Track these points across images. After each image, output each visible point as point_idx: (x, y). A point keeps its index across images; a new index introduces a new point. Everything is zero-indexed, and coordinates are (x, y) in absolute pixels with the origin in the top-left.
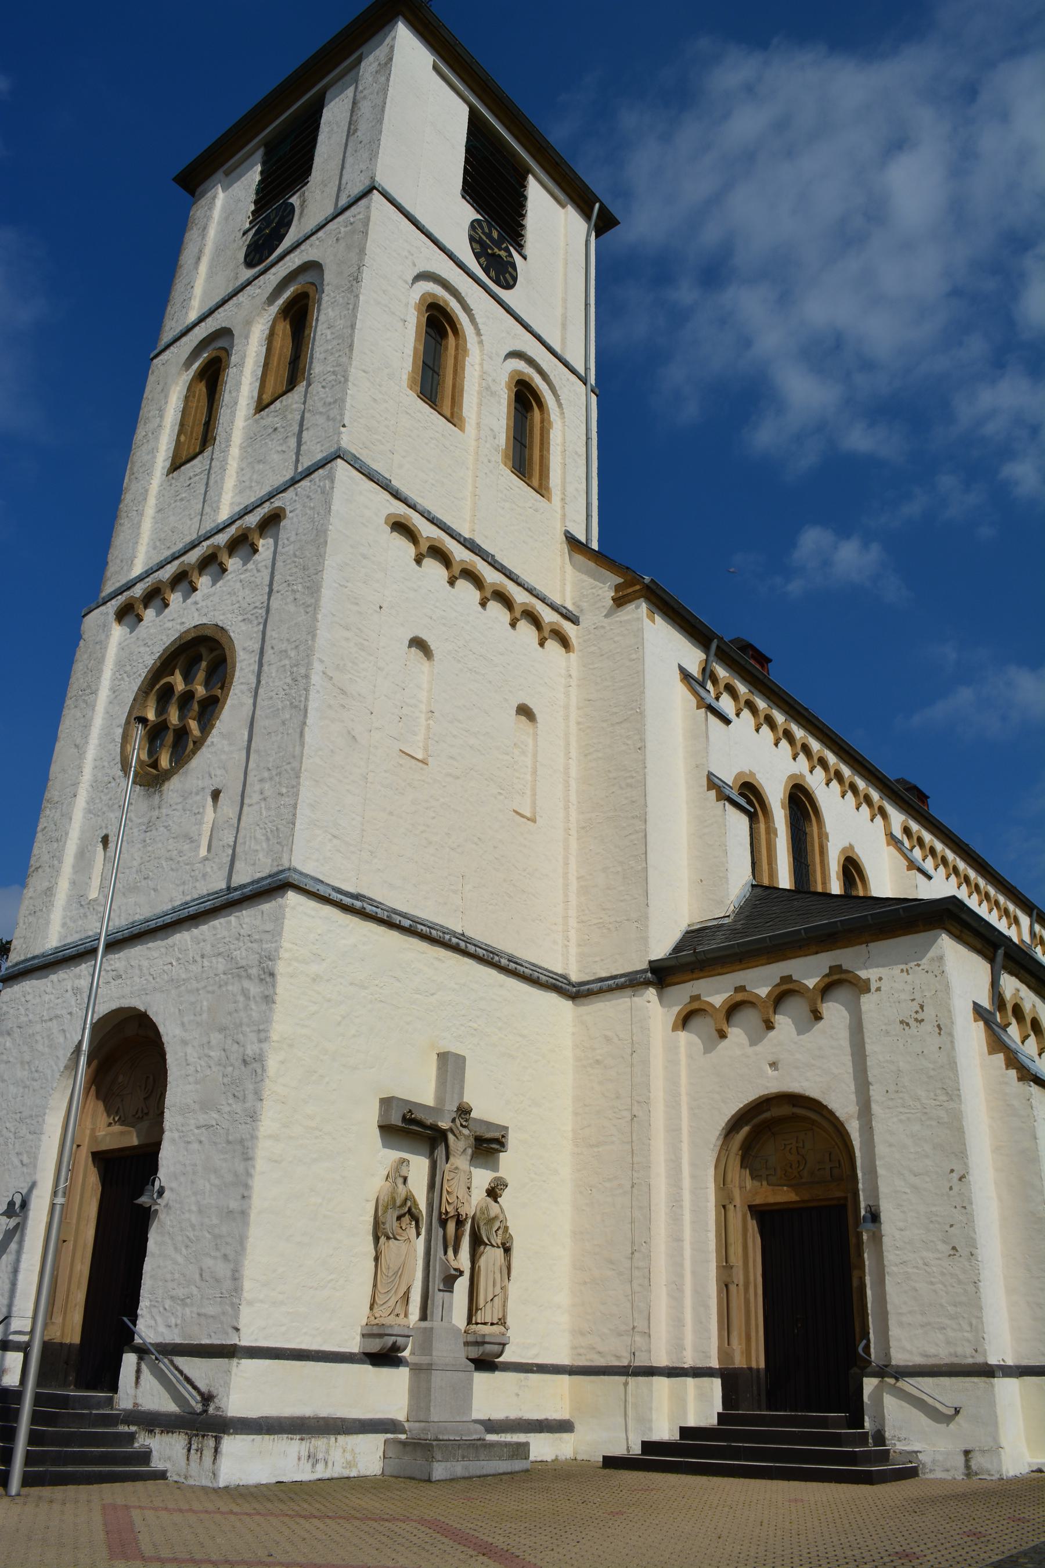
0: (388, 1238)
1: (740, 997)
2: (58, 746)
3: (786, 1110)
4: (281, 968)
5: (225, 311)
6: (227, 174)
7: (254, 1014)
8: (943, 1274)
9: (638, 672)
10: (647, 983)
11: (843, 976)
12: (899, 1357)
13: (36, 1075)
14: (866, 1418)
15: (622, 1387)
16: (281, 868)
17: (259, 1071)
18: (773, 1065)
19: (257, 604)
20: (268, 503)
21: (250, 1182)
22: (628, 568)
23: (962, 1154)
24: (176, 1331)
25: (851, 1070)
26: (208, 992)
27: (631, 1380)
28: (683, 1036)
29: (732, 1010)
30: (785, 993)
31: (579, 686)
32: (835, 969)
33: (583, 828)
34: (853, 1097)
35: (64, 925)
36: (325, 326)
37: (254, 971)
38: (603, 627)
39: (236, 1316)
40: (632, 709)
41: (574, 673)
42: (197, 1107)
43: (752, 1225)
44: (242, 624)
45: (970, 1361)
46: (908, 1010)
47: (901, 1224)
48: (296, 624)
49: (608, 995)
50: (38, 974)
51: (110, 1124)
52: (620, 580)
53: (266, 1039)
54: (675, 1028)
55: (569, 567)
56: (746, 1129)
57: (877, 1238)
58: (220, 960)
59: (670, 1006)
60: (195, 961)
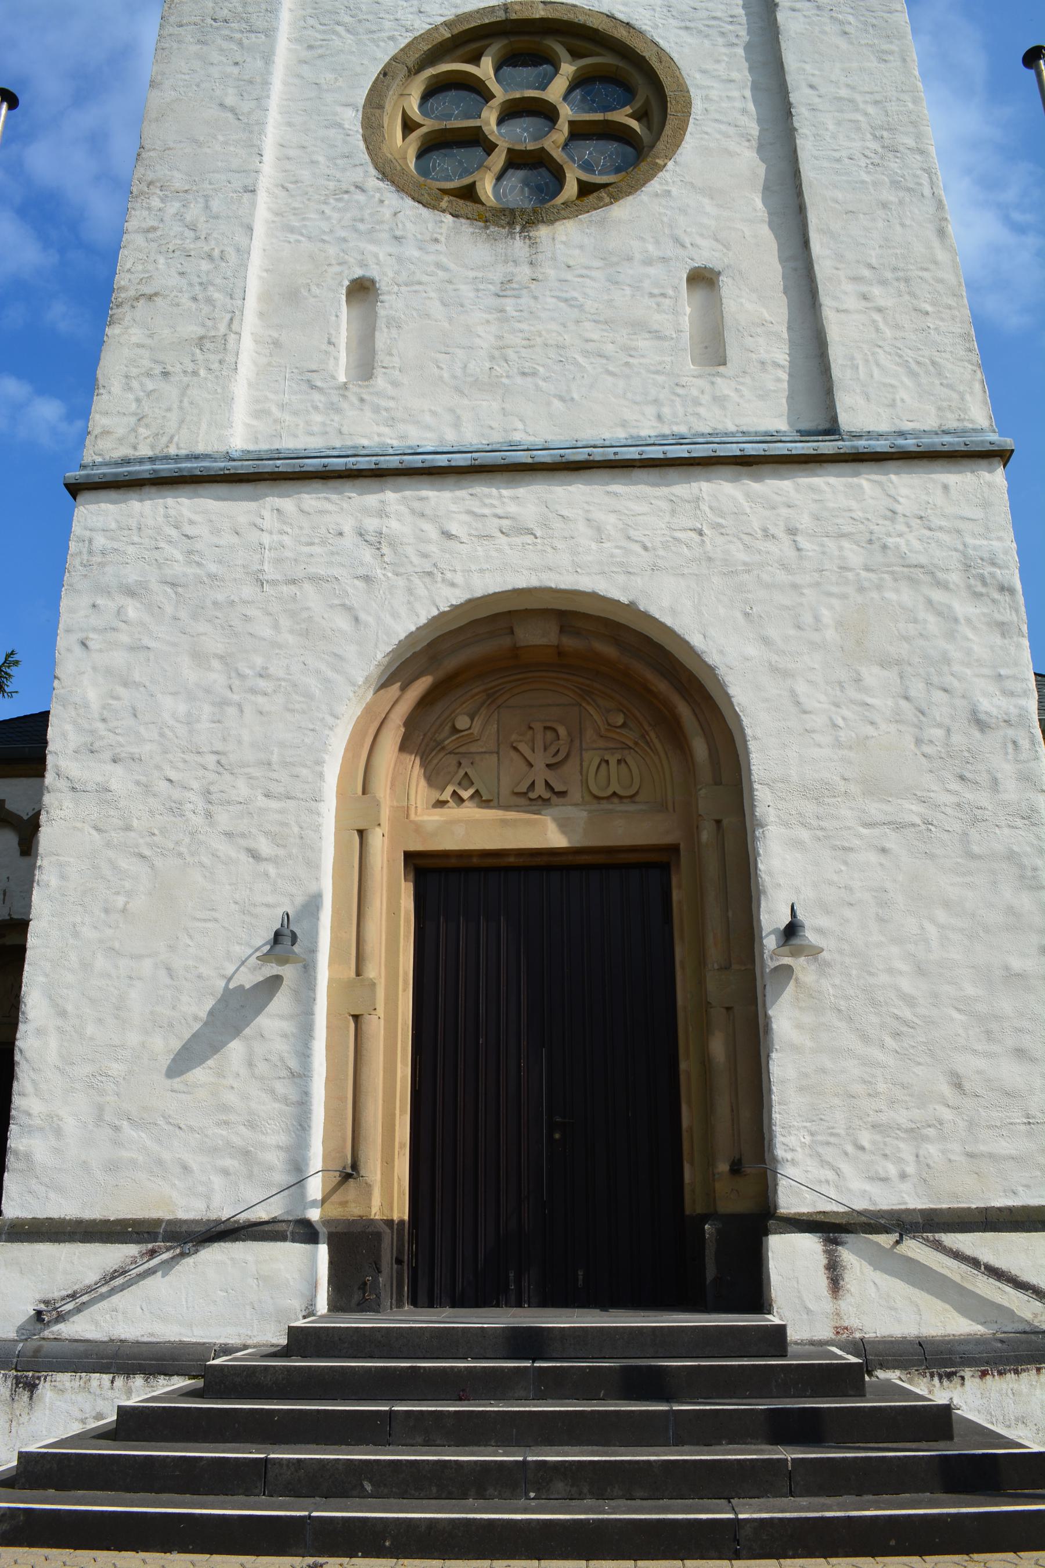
7: (976, 648)
13: (262, 684)
24: (906, 1187)
26: (830, 594)
35: (259, 414)
44: (682, 33)
51: (441, 804)
58: (846, 544)
60: (767, 535)
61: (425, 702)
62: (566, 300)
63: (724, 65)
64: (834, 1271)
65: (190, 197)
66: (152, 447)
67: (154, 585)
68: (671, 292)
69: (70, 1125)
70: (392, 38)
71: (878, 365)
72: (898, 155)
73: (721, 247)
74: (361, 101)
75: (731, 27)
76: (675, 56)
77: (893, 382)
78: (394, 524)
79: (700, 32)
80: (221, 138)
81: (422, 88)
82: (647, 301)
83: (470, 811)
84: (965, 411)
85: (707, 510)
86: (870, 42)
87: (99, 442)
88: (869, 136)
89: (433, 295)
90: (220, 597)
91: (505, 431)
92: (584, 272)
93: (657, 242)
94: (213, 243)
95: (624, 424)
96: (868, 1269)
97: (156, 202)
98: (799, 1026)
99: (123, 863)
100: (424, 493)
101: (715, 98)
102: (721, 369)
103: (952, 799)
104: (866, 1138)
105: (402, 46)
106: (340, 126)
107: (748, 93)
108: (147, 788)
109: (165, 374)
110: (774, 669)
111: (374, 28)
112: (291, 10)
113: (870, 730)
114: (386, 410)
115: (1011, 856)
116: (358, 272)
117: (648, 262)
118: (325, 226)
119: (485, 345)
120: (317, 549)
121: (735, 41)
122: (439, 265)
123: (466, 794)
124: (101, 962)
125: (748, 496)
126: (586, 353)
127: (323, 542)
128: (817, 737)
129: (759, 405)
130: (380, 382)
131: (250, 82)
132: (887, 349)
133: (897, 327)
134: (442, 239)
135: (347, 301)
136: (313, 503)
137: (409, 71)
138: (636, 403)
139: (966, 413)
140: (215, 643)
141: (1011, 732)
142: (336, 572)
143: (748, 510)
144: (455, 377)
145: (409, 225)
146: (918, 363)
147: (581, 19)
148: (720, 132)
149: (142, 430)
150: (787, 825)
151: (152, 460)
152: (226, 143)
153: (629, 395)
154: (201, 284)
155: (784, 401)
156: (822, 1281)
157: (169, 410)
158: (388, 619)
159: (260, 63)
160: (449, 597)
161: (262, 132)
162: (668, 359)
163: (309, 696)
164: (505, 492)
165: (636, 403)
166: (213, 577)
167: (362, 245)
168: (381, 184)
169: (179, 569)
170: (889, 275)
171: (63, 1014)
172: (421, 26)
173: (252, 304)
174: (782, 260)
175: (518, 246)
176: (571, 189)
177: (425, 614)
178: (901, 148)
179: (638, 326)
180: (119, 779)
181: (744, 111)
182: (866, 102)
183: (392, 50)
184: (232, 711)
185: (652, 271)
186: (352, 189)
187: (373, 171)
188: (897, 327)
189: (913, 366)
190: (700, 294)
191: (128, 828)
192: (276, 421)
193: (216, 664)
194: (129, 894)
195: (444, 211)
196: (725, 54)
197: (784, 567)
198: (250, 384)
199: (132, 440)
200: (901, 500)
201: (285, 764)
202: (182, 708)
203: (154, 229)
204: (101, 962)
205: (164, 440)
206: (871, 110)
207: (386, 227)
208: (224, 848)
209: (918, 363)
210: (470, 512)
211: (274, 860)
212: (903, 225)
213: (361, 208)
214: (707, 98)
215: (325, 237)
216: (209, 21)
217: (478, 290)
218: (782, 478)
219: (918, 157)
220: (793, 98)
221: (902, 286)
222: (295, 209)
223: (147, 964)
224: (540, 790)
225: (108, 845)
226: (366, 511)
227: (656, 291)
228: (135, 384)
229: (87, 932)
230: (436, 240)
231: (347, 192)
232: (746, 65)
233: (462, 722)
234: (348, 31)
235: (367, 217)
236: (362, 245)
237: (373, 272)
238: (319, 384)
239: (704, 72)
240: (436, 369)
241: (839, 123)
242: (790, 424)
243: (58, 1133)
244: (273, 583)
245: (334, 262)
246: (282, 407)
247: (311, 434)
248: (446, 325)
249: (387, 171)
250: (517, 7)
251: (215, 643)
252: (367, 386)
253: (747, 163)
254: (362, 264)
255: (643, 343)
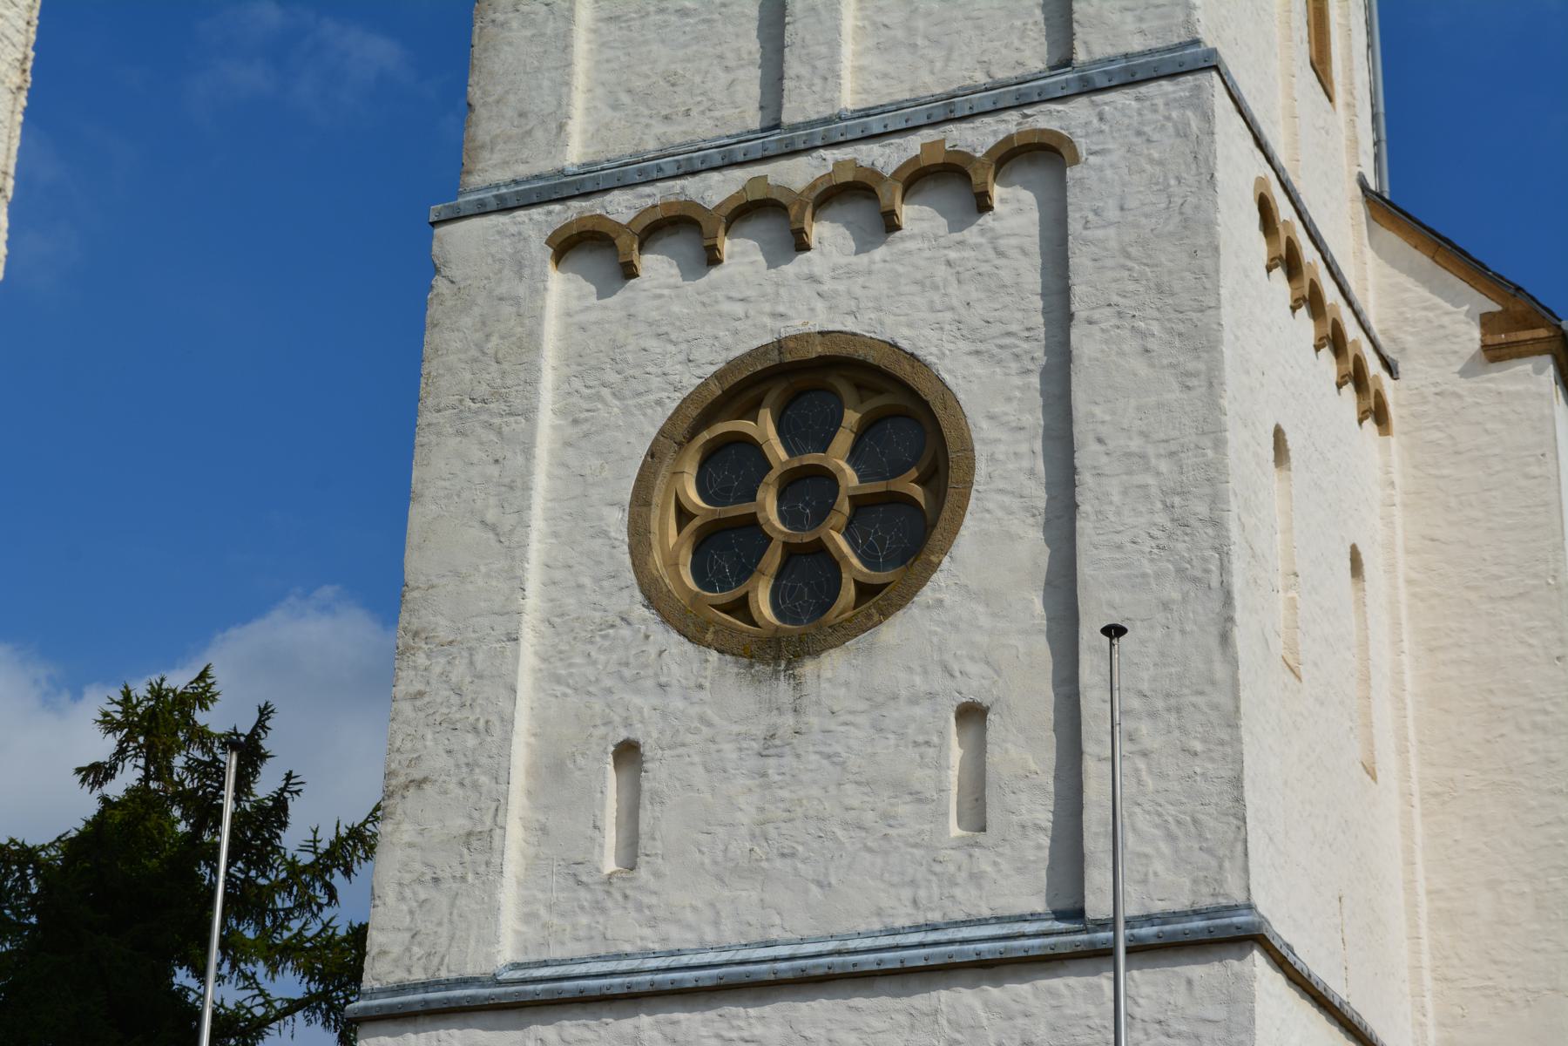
2: (418, 516)
9: (1546, 504)
16: (1223, 902)
19: (1014, 328)
20: (1014, 116)
22: (1519, 289)
31: (1405, 505)
33: (1436, 795)
35: (528, 917)
40: (1536, 576)
41: (1397, 478)
44: (972, 360)
48: (1160, 405)
50: (489, 1018)
52: (1494, 307)
55: (1369, 254)
62: (829, 757)
63: (1015, 403)
65: (454, 650)
66: (425, 969)
68: (935, 739)
70: (659, 402)
71: (1134, 829)
72: (1188, 530)
73: (991, 672)
74: (628, 497)
75: (1026, 346)
76: (961, 396)
77: (1148, 850)
79: (992, 356)
80: (483, 569)
81: (698, 457)
82: (912, 753)
84: (1220, 882)
85: (945, 1023)
86: (1174, 361)
87: (377, 965)
88: (1159, 505)
89: (696, 759)
91: (763, 927)
92: (850, 718)
94: (478, 710)
95: (879, 913)
97: (421, 659)
100: (677, 1016)
101: (1001, 457)
105: (670, 413)
107: (1038, 446)
109: (436, 880)
111: (642, 388)
112: (554, 368)
114: (649, 907)
116: (623, 734)
117: (914, 701)
118: (590, 672)
119: (746, 821)
121: (1031, 367)
125: (986, 1005)
126: (845, 825)
129: (1015, 888)
130: (643, 873)
132: (1146, 807)
133: (1162, 776)
134: (707, 685)
135: (616, 767)
136: (574, 1031)
137: (680, 444)
138: (893, 885)
139: (1221, 886)
143: (985, 1022)
144: (715, 863)
145: (675, 668)
146: (1179, 822)
147: (861, 353)
148: (1003, 507)
149: (415, 949)
152: (488, 575)
153: (887, 875)
154: (467, 765)
155: (1044, 873)
157: (440, 924)
159: (520, 459)
161: (524, 559)
162: (927, 827)
164: (752, 1011)
165: (893, 885)
167: (627, 697)
168: (646, 613)
170: (1160, 704)
173: (519, 780)
174: (1055, 686)
176: (848, 593)
178: (1192, 522)
179: (900, 787)
181: (1032, 473)
182: (1159, 456)
183: (660, 418)
185: (918, 711)
186: (618, 622)
187: (639, 596)
188: (1162, 776)
189: (1173, 827)
190: (971, 732)
192: (545, 926)
195: (709, 646)
196: (1018, 388)
198: (519, 883)
199: (407, 962)
200: (1141, 1001)
203: (421, 694)
205: (436, 960)
206: (1164, 466)
207: (651, 672)
209: (1179, 822)
210: (719, 1036)
212: (1183, 632)
213: (627, 648)
214: (992, 458)
215: (591, 689)
216: (468, 402)
217: (740, 750)
218: (1023, 981)
219: (1210, 531)
221: (1173, 718)
222: (561, 652)
227: (920, 739)
228: (408, 893)
230: (701, 687)
231: (612, 626)
232: (1040, 401)
234: (614, 394)
235: (632, 660)
236: (627, 697)
237: (637, 734)
238: (584, 878)
240: (697, 855)
241: (1125, 493)
242: (1049, 903)
245: (598, 722)
247: (578, 939)
248: (708, 796)
249: (653, 595)
250: (792, 345)
252: (630, 879)
253: (1032, 546)
254: (627, 724)
255: (904, 809)
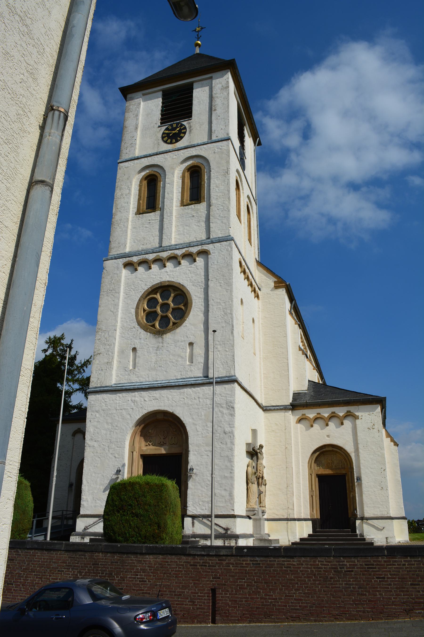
0: (252, 483)
1: (318, 416)
2: (100, 309)
3: (330, 449)
4: (236, 406)
5: (158, 158)
6: (144, 95)
7: (226, 419)
8: (379, 494)
10: (290, 409)
11: (351, 414)
12: (367, 515)
13: (117, 428)
14: (357, 530)
15: (286, 524)
17: (232, 436)
18: (328, 436)
20: (200, 246)
21: (233, 468)
23: (384, 464)
24: (206, 511)
25: (352, 439)
26: (204, 410)
27: (289, 522)
28: (299, 425)
29: (316, 419)
30: (333, 416)
32: (348, 412)
34: (353, 447)
35: (117, 376)
36: (214, 185)
37: (224, 406)
38: (270, 294)
39: (233, 506)
41: (260, 307)
42: (204, 445)
43: (317, 479)
44: (193, 286)
45: (386, 516)
46: (370, 425)
47: (368, 481)
49: (276, 411)
50: (111, 393)
51: (147, 446)
53: (234, 427)
54: (296, 423)
55: (257, 271)
56: (318, 453)
57: (360, 485)
58: (207, 400)
59: (296, 416)
60: (195, 399)
61: (143, 428)
64: (193, 523)
67: (101, 411)
69: (89, 500)
70: (141, 292)
78: (137, 399)
82: (181, 350)
83: (152, 447)
90: (110, 413)
93: (184, 337)
95: (175, 376)
96: (198, 523)
97: (100, 333)
98: (192, 485)
99: (97, 459)
102: (192, 364)
103: (219, 446)
104: (201, 503)
106: (131, 313)
108: (100, 446)
110: (194, 424)
113: (208, 434)
115: (227, 456)
116: (133, 346)
117: (182, 342)
120: (125, 404)
122: (147, 344)
123: (150, 444)
124: (93, 475)
126: (170, 362)
127: (126, 402)
128: (199, 436)
130: (136, 369)
131: (116, 305)
133: (222, 355)
140: (110, 421)
141: (230, 434)
142: (128, 408)
147: (174, 285)
150: (193, 451)
151: (100, 387)
156: (191, 525)
158: (135, 416)
159: (117, 300)
160: (145, 412)
163: (123, 430)
164: (154, 392)
166: (109, 409)
167: (134, 340)
169: (104, 407)
170: (221, 343)
171: (88, 483)
172: (146, 288)
175: (160, 339)
176: (171, 324)
177: (141, 415)
180: (96, 444)
183: (141, 294)
184: (112, 433)
185: (182, 343)
187: (137, 324)
188: (222, 355)
190: (191, 347)
191: (97, 453)
192: (120, 378)
193: (110, 424)
194: (97, 463)
197: (197, 404)
201: (120, 442)
202: (105, 432)
203: (100, 339)
204: (93, 475)
206: (223, 304)
208: (111, 456)
211: (118, 458)
214: (195, 302)
220: (210, 303)
223: (100, 475)
224: (162, 443)
225: (94, 455)
226: (132, 396)
229: (91, 470)
233: (150, 431)
237: (136, 346)
239: (195, 296)
243: (88, 501)
244: (118, 410)
246: (121, 375)
249: (139, 323)
251: (110, 421)
253: (201, 317)
254: (134, 345)
255: (180, 359)
